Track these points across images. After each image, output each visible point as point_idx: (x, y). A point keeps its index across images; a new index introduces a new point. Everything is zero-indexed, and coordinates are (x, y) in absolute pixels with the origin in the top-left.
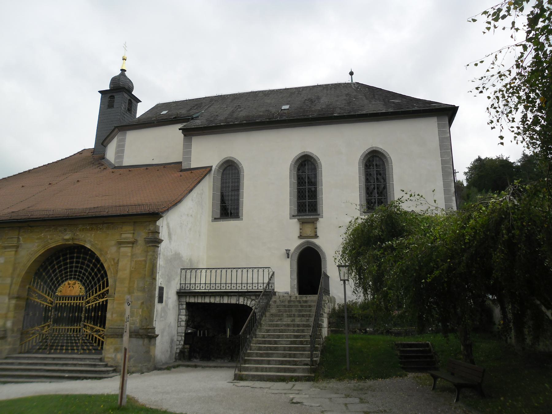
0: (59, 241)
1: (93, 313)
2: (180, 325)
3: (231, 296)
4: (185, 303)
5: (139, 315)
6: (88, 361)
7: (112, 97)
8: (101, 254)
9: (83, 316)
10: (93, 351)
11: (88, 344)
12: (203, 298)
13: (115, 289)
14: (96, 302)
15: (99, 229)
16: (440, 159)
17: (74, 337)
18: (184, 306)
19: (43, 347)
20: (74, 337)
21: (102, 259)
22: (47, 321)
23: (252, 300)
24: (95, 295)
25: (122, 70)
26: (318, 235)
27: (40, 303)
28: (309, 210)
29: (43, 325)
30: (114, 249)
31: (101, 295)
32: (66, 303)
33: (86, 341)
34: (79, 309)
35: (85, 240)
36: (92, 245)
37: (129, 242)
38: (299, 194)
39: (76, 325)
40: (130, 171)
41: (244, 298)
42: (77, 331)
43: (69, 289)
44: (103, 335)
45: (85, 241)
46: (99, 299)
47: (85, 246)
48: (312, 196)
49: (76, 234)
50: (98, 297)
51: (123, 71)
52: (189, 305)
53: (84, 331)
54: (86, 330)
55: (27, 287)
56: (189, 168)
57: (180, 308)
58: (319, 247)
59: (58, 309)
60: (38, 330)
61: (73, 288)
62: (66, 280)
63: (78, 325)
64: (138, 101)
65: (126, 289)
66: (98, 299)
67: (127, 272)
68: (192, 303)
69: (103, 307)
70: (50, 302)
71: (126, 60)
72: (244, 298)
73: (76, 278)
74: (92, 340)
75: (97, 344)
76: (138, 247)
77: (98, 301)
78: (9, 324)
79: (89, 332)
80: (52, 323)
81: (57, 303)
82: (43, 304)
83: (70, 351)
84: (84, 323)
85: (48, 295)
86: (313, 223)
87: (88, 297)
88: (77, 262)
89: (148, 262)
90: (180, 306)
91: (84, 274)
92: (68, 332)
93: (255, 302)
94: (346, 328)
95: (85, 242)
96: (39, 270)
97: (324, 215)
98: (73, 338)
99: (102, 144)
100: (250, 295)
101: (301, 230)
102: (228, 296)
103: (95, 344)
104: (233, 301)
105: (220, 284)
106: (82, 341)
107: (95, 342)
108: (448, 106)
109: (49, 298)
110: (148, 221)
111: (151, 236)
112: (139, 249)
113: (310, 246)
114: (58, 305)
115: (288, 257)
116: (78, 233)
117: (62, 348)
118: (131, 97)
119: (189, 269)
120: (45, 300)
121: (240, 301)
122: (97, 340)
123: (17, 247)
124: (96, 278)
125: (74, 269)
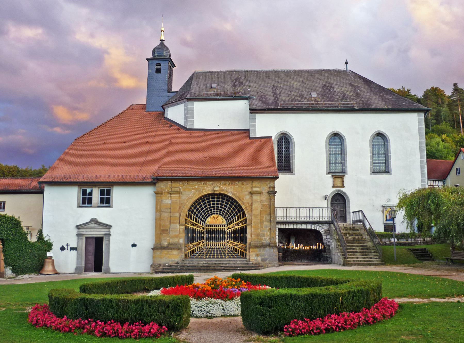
3: (307, 224)
4: (278, 228)
8: (240, 200)
9: (226, 236)
11: (232, 253)
13: (252, 221)
16: (419, 141)
17: (221, 248)
20: (221, 248)
21: (240, 203)
22: (202, 239)
28: (285, 169)
29: (199, 242)
30: (248, 197)
33: (230, 251)
36: (233, 194)
39: (222, 241)
42: (223, 245)
45: (228, 192)
47: (228, 194)
52: (280, 229)
54: (229, 244)
58: (345, 194)
59: (209, 232)
60: (196, 245)
65: (259, 221)
66: (235, 226)
67: (259, 211)
68: (287, 228)
69: (244, 230)
70: (201, 228)
74: (234, 250)
80: (205, 240)
82: (198, 229)
83: (220, 257)
85: (200, 224)
89: (271, 205)
91: (224, 211)
92: (217, 246)
97: (348, 173)
98: (221, 249)
103: (236, 253)
104: (308, 227)
107: (236, 251)
109: (201, 225)
112: (265, 197)
120: (198, 227)
121: (312, 227)
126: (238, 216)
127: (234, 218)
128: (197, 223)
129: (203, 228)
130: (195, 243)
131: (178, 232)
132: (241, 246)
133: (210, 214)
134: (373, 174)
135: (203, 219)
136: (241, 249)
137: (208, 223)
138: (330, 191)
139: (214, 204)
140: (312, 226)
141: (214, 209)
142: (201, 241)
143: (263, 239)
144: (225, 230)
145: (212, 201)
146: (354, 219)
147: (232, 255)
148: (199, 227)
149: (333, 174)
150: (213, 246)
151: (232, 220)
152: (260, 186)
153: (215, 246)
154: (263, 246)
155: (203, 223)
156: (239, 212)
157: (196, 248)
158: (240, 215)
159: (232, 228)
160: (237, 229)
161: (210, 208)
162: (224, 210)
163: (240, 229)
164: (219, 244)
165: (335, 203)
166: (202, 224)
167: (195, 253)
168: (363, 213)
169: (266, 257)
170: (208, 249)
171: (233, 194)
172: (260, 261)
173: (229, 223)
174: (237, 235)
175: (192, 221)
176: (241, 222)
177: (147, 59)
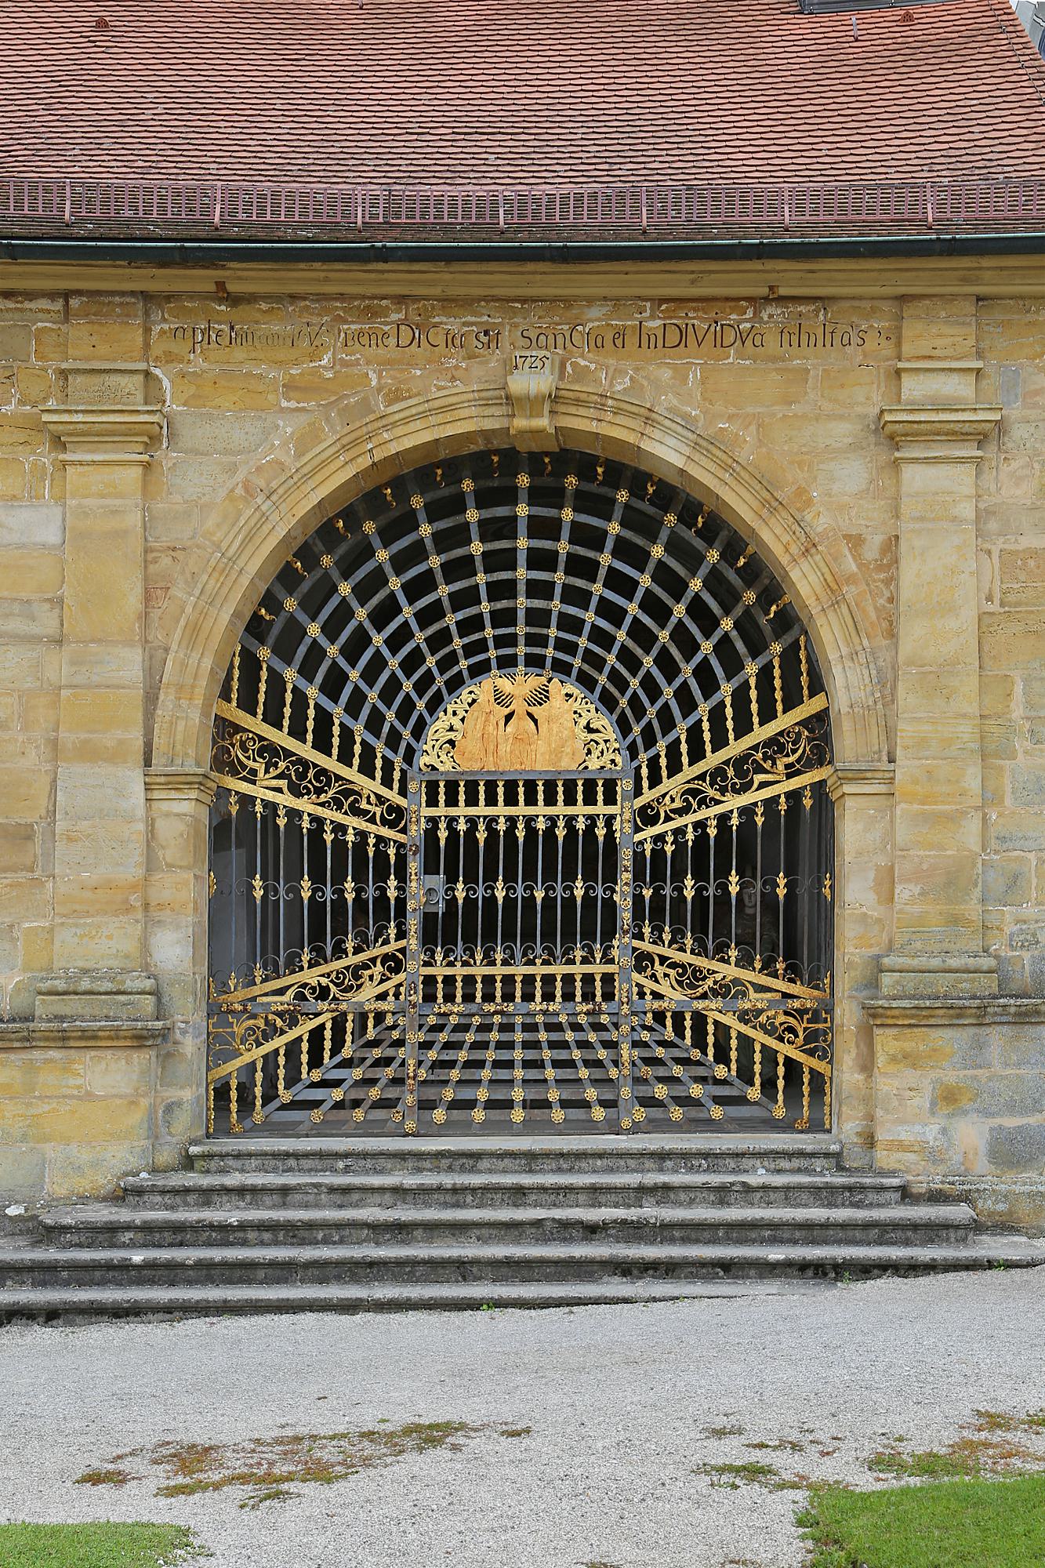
1: (689, 882)
6: (762, 1171)
8: (773, 505)
11: (677, 1071)
13: (890, 732)
17: (576, 1027)
19: (374, 1093)
20: (576, 1027)
24: (689, 772)
29: (352, 960)
31: (731, 772)
32: (494, 819)
33: (660, 1052)
36: (703, 444)
39: (579, 954)
40: (102, 24)
42: (588, 997)
43: (509, 729)
46: (723, 791)
47: (646, 445)
49: (569, 369)
54: (649, 985)
61: (535, 722)
65: (966, 731)
66: (711, 793)
74: (700, 1043)
75: (734, 1066)
76: (1014, 465)
79: (675, 996)
80: (413, 943)
81: (433, 821)
84: (636, 943)
85: (367, 769)
87: (645, 784)
88: (541, 560)
92: (528, 997)
94: (362, 957)
95: (648, 420)
98: (570, 1036)
103: (721, 1071)
106: (636, 1052)
109: (371, 786)
114: (443, 834)
116: (583, 363)
117: (500, 1095)
122: (734, 1043)
128: (331, 764)
139: (507, 559)
141: (503, 618)
142: (378, 951)
144: (610, 835)
150: (489, 997)
152: (979, 355)
153: (508, 997)
155: (398, 761)
157: (326, 1019)
160: (735, 821)
162: (603, 624)
163: (759, 820)
164: (548, 980)
166: (388, 765)
167: (316, 1075)
170: (443, 1037)
171: (703, 444)
173: (653, 763)
175: (281, 738)
176: (775, 745)
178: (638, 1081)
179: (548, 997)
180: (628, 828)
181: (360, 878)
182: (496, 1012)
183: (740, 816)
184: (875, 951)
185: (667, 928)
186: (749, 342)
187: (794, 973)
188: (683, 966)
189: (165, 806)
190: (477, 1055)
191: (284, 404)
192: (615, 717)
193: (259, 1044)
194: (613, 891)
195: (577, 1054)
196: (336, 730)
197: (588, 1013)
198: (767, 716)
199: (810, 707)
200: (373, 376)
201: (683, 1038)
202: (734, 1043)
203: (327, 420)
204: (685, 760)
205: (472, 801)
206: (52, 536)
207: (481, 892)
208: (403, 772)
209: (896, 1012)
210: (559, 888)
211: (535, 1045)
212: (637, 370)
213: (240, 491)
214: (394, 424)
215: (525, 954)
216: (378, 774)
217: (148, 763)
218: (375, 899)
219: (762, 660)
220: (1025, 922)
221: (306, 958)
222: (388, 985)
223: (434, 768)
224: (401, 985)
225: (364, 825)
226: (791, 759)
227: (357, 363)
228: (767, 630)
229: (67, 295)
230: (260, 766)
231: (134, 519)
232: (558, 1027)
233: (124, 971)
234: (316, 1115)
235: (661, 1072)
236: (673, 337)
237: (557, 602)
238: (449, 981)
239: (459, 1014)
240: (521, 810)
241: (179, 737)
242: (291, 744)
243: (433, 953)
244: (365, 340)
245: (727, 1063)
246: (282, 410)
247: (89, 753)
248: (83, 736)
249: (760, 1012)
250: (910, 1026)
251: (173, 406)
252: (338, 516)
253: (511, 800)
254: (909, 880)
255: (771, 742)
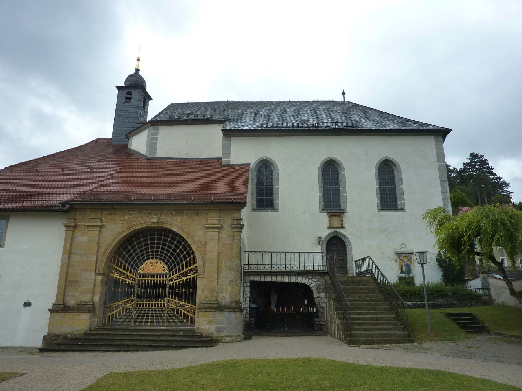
0: (144, 223)
1: (177, 290)
2: (245, 301)
3: (291, 275)
5: (228, 291)
7: (129, 93)
9: (167, 292)
10: (179, 324)
11: (174, 317)
12: (266, 277)
14: (179, 280)
15: (184, 214)
17: (159, 311)
18: (249, 284)
19: (128, 320)
20: (159, 311)
21: (189, 241)
22: (131, 296)
23: (309, 279)
24: (178, 274)
25: (135, 69)
26: (344, 226)
27: (122, 280)
28: (266, 206)
29: (126, 300)
31: (184, 274)
32: (149, 280)
33: (171, 315)
34: (163, 285)
35: (172, 224)
36: (180, 228)
37: (217, 227)
38: (258, 192)
39: (160, 300)
41: (302, 278)
42: (161, 306)
44: (188, 309)
45: (172, 225)
46: (183, 277)
48: (269, 194)
49: (161, 218)
50: (181, 275)
51: (137, 70)
52: (252, 282)
53: (169, 306)
54: (170, 305)
55: (109, 264)
56: (229, 164)
57: (245, 285)
59: (142, 285)
60: (121, 305)
61: (156, 266)
62: (148, 259)
63: (163, 300)
64: (150, 99)
66: (181, 277)
69: (193, 283)
71: (139, 60)
72: (302, 278)
73: (158, 258)
74: (177, 313)
75: (182, 317)
77: (182, 279)
78: (97, 299)
79: (174, 306)
80: (135, 298)
81: (140, 280)
82: (126, 281)
83: (155, 324)
84: (169, 298)
85: (130, 273)
86: (340, 216)
87: (171, 275)
88: (158, 243)
90: (245, 284)
91: (167, 255)
92: (152, 306)
93: (312, 281)
96: (119, 249)
97: (348, 209)
98: (158, 312)
99: (126, 136)
100: (308, 275)
101: (330, 222)
102: (288, 275)
103: (180, 318)
104: (293, 279)
105: (262, 265)
106: (168, 315)
107: (181, 316)
108: (436, 128)
109: (131, 275)
110: (232, 210)
111: (236, 222)
113: (337, 235)
114: (141, 282)
115: (319, 244)
116: (163, 217)
118: (145, 95)
119: (252, 252)
120: (127, 277)
121: (299, 280)
122: (183, 313)
123: (101, 227)
124: (179, 258)
125: (160, 249)
126: (187, 261)
127: (180, 265)
128: (125, 272)
129: (134, 280)
130: (120, 303)
131: (92, 285)
132: (189, 308)
133: (146, 258)
134: (381, 211)
135: (134, 265)
136: (188, 312)
137: (142, 272)
138: (325, 233)
139: (153, 243)
140: (298, 278)
143: (221, 297)
144: (166, 282)
145: (151, 239)
146: (358, 271)
147: (174, 321)
148: (129, 278)
149: (329, 211)
150: (146, 306)
151: (177, 268)
152: (219, 217)
153: (149, 306)
154: (220, 308)
155: (135, 272)
156: (189, 256)
158: (190, 260)
159: (176, 279)
160: (184, 281)
161: (146, 249)
162: (166, 252)
163: (188, 281)
164: (155, 304)
165: (332, 250)
166: (133, 272)
167: (119, 317)
168: (372, 260)
169: (225, 325)
170: (139, 312)
171: (180, 228)
172: (214, 332)
173: (173, 272)
174: (184, 291)
175: (119, 268)
176: (191, 270)
177: (117, 87)
178: (168, 319)
179: (155, 306)
180: (168, 282)
181: (128, 289)
182: (147, 308)
183: (185, 280)
184: (201, 300)
185: (173, 296)
186: (187, 215)
187: (192, 303)
188: (175, 302)
189: (98, 278)
190: (144, 315)
191: (120, 223)
192: (167, 266)
193: (111, 312)
194: (166, 291)
195: (159, 315)
196: (126, 267)
197: (161, 309)
198: (190, 266)
199: (195, 265)
200: (133, 219)
201: (175, 313)
202: (183, 313)
203: (126, 225)
204: (177, 272)
205: (146, 277)
206: (86, 240)
207: (146, 291)
208: (136, 273)
209: (202, 309)
210: (152, 290)
211: (153, 313)
212: (171, 218)
213: (113, 234)
214: (135, 226)
215: (152, 300)
216: (132, 273)
217: (95, 272)
218: (174, 292)
219: (190, 258)
220: (223, 296)
221: (119, 300)
222: (131, 304)
223: (140, 273)
224: (133, 304)
225: (129, 281)
226: (193, 272)
227: (131, 217)
228: (191, 254)
229: (91, 209)
230: (115, 272)
231: (97, 238)
232: (156, 311)
233: (89, 301)
234: (119, 323)
235: (171, 318)
236: (176, 214)
237: (160, 249)
238: (140, 304)
239: (141, 309)
240: (153, 279)
241: (101, 268)
242: (120, 269)
243: (138, 299)
244: (132, 214)
245: (181, 316)
246: (120, 224)
247: (87, 270)
248: (87, 268)
249: (187, 309)
250: (204, 311)
251: (104, 223)
252: (129, 237)
253: (163, 277)
254: (206, 290)
255: (190, 270)
